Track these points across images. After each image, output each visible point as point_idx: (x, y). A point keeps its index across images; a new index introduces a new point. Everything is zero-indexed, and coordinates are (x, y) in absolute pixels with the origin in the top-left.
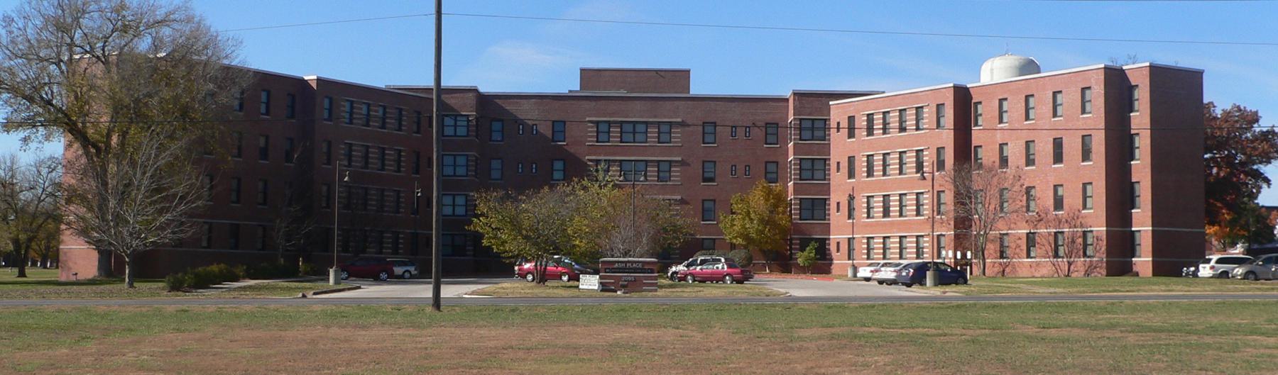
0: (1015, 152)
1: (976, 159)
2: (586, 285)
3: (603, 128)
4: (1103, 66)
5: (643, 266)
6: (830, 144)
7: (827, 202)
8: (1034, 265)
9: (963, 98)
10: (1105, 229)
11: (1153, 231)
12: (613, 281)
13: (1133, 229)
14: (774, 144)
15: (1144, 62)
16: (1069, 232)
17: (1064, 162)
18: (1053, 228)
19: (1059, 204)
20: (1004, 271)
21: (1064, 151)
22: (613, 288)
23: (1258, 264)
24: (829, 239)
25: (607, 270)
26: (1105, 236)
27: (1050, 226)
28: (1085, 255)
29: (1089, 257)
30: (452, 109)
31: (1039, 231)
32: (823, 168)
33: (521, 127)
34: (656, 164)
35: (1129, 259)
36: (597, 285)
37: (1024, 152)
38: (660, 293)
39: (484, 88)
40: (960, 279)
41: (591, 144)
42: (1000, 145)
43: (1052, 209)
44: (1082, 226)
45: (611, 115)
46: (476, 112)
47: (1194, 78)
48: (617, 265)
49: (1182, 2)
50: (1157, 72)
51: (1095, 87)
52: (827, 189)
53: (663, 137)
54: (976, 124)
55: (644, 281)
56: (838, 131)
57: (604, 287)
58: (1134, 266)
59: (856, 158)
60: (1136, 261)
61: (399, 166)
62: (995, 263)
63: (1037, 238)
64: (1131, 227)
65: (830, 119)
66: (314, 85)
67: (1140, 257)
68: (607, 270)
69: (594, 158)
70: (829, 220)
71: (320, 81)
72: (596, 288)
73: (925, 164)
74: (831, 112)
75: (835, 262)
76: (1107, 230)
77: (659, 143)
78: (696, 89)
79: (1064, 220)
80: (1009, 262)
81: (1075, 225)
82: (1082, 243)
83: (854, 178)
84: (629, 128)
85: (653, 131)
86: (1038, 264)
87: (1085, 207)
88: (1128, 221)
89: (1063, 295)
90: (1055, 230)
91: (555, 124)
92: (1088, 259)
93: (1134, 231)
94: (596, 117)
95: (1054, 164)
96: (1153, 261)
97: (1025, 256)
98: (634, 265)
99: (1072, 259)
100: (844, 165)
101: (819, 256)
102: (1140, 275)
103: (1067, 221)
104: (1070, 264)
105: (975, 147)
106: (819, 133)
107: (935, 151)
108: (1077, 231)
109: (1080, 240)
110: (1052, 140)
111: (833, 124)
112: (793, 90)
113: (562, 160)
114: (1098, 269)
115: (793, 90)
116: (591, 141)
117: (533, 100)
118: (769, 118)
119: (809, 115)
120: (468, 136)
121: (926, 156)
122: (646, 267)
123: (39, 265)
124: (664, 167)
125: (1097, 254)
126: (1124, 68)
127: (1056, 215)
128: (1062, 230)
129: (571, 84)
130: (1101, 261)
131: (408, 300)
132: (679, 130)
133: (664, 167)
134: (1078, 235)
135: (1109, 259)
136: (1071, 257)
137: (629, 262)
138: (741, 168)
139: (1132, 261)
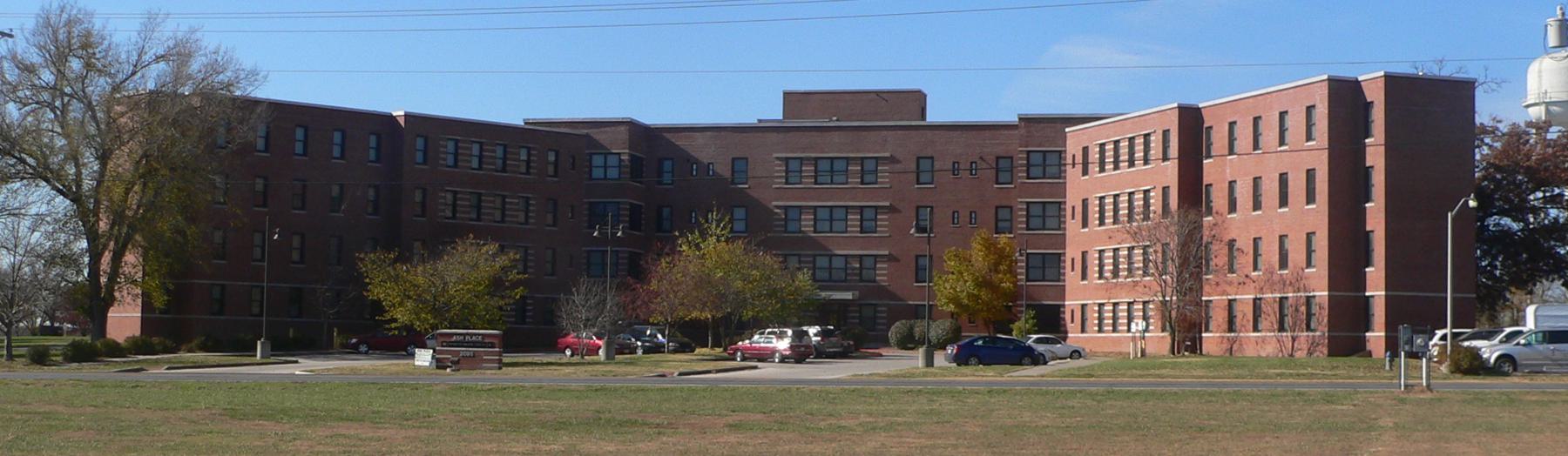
1: (1209, 201)
4: (1325, 77)
5: (483, 338)
6: (1065, 183)
7: (1062, 258)
8: (1260, 340)
9: (1192, 122)
10: (1326, 293)
11: (1386, 296)
13: (1367, 294)
15: (1321, 75)
16: (1293, 297)
19: (1283, 263)
20: (1231, 348)
21: (1289, 190)
23: (1518, 344)
24: (1064, 306)
25: (444, 344)
28: (1308, 328)
30: (602, 147)
31: (1264, 296)
32: (1057, 214)
33: (695, 166)
34: (859, 211)
35: (1362, 334)
38: (767, 371)
40: (1026, 359)
41: (777, 186)
43: (1277, 267)
44: (1305, 291)
46: (630, 150)
47: (1460, 93)
48: (455, 338)
49: (1142, 2)
50: (1392, 81)
52: (1061, 241)
53: (868, 178)
55: (485, 357)
56: (1074, 167)
57: (440, 364)
58: (1367, 344)
60: (1370, 336)
61: (527, 217)
62: (1223, 337)
63: (1263, 305)
64: (1365, 290)
65: (1065, 151)
66: (402, 122)
67: (1373, 331)
68: (444, 344)
70: (1064, 281)
71: (407, 116)
72: (427, 364)
74: (1068, 142)
75: (1069, 335)
76: (1329, 295)
77: (1028, 178)
78: (934, 115)
79: (1288, 282)
80: (1236, 337)
86: (1264, 339)
87: (1309, 265)
88: (1361, 283)
89: (877, 378)
90: (1279, 295)
91: (1010, 160)
92: (1311, 334)
93: (1368, 297)
94: (837, 152)
96: (1386, 337)
97: (1251, 329)
98: (474, 338)
99: (1296, 334)
100: (1079, 210)
101: (1036, 328)
102: (1374, 356)
104: (1294, 339)
105: (1207, 186)
106: (1054, 170)
109: (1303, 309)
110: (1278, 175)
111: (1069, 160)
112: (1019, 115)
113: (743, 206)
114: (1320, 347)
115: (1019, 115)
116: (779, 183)
118: (1001, 151)
119: (1040, 146)
120: (620, 178)
122: (486, 341)
124: (868, 214)
125: (1320, 327)
126: (1360, 79)
127: (1281, 275)
129: (774, 111)
133: (868, 214)
136: (1294, 331)
137: (467, 334)
138: (964, 216)
139: (1365, 337)
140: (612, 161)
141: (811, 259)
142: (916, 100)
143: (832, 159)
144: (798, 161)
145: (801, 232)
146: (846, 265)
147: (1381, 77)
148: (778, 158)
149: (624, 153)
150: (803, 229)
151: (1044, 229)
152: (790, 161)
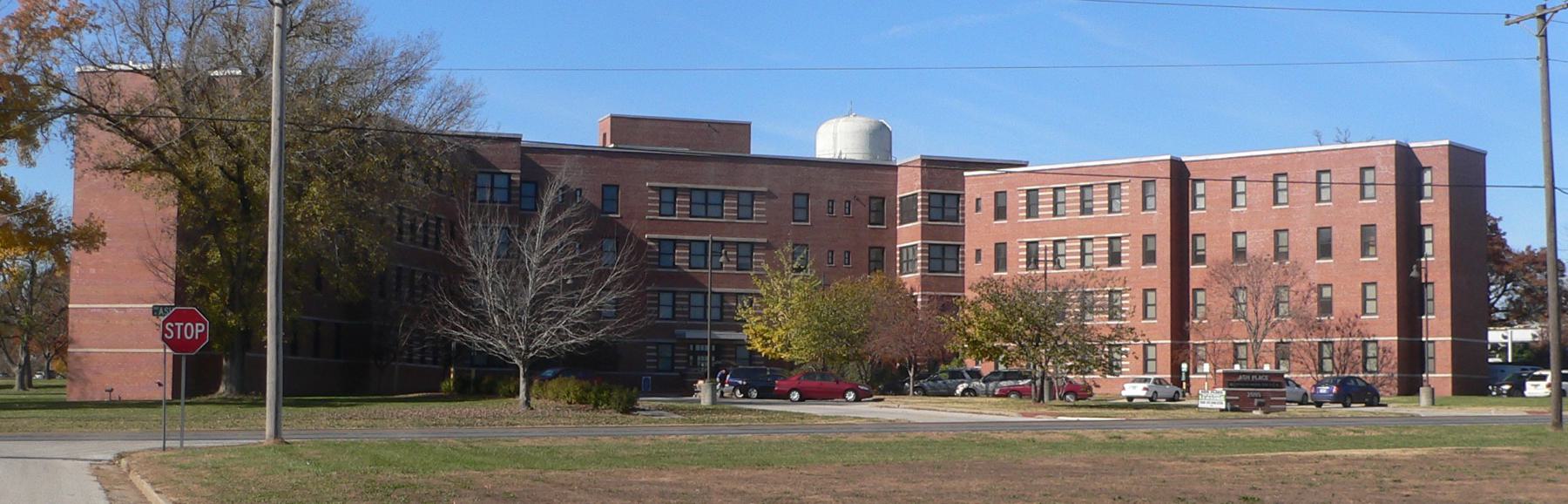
0: (1303, 242)
2: (1208, 403)
3: (668, 196)
4: (1394, 142)
11: (1453, 341)
12: (1237, 398)
14: (802, 221)
15: (1442, 139)
16: (1341, 341)
17: (1333, 256)
18: (1318, 337)
22: (1237, 406)
25: (1231, 384)
26: (1396, 348)
27: (1311, 334)
29: (1371, 372)
31: (1294, 340)
34: (735, 247)
36: (1224, 402)
37: (1273, 244)
39: (530, 136)
41: (651, 217)
42: (1234, 234)
44: (1360, 334)
45: (678, 180)
51: (1382, 167)
54: (1194, 208)
55: (1272, 398)
59: (1008, 245)
65: (964, 194)
67: (1434, 372)
68: (1231, 384)
69: (656, 236)
73: (1123, 255)
74: (966, 185)
78: (758, 148)
79: (1333, 327)
81: (1350, 334)
82: (1361, 356)
83: (1006, 270)
84: (699, 197)
85: (730, 204)
87: (1364, 312)
95: (1318, 259)
96: (1453, 378)
98: (1260, 378)
103: (1338, 329)
107: (1141, 239)
108: (1354, 341)
109: (1359, 352)
110: (1316, 230)
114: (1385, 387)
115: (922, 156)
117: (577, 156)
118: (875, 191)
121: (1126, 244)
123: (1564, 372)
128: (1331, 340)
130: (1391, 377)
131: (916, 425)
132: (764, 203)
134: (1355, 345)
135: (1401, 375)
140: (501, 182)
141: (687, 296)
142: (742, 130)
143: (706, 191)
144: (749, 195)
145: (675, 267)
146: (722, 304)
147: (1392, 145)
148: (652, 188)
149: (515, 174)
150: (676, 264)
151: (943, 271)
152: (663, 191)
